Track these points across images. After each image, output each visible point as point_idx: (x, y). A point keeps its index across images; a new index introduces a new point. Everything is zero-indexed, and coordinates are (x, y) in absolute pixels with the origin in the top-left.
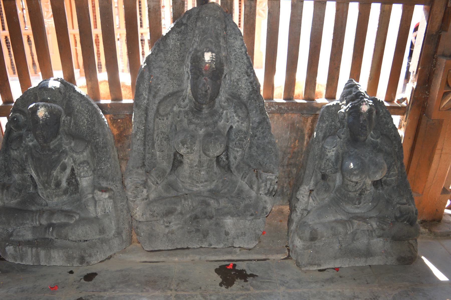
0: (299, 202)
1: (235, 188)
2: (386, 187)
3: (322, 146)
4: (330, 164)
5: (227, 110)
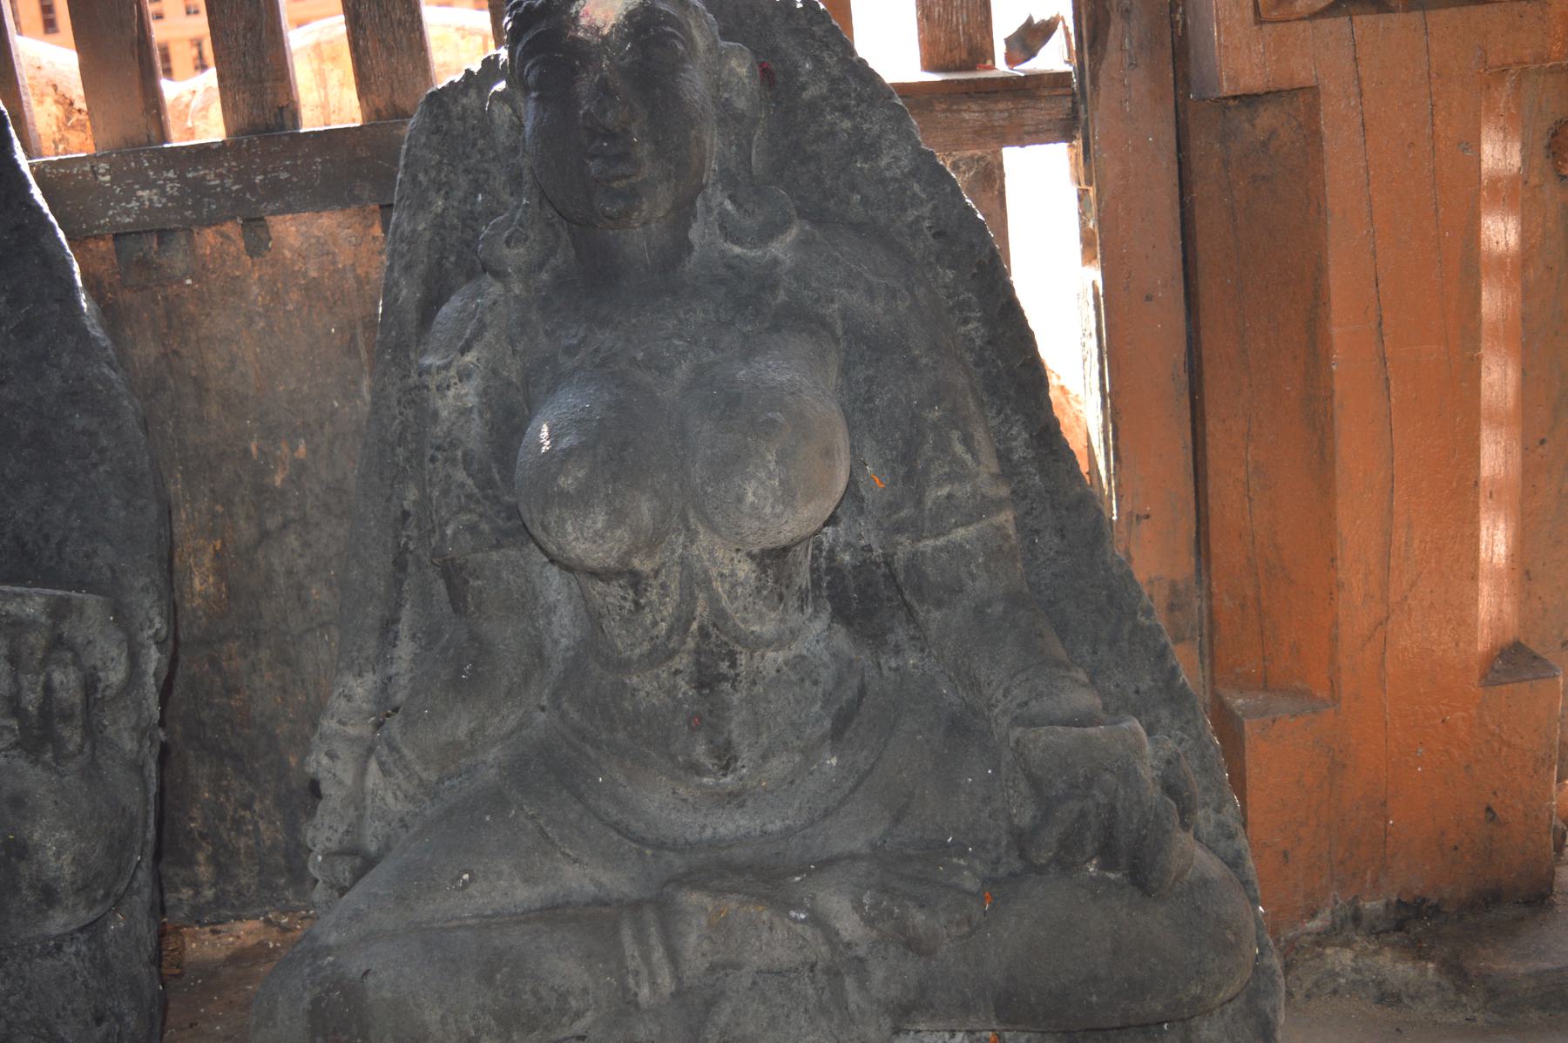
2: (934, 617)
4: (460, 475)
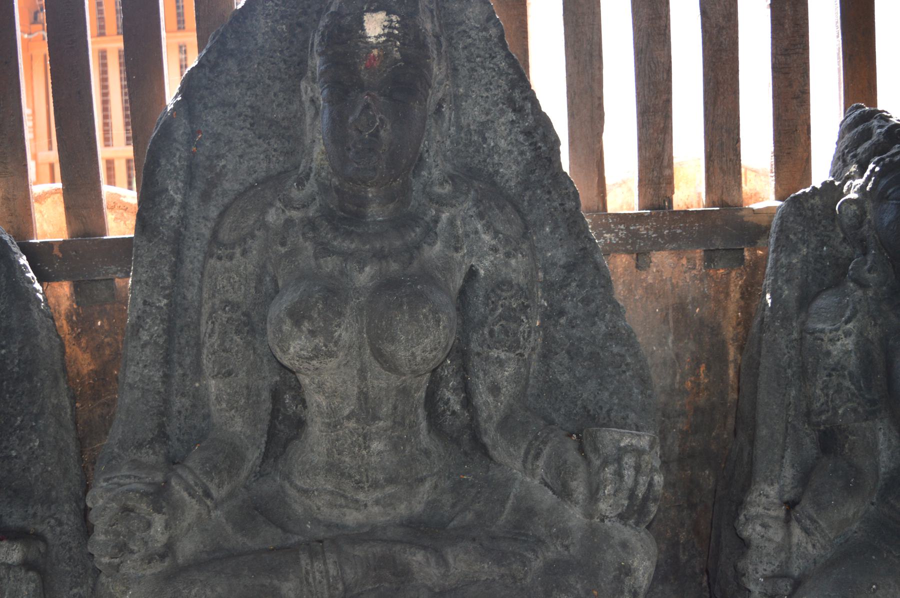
0: (753, 555)
1: (503, 503)
3: (803, 331)
4: (847, 383)
5: (453, 206)
